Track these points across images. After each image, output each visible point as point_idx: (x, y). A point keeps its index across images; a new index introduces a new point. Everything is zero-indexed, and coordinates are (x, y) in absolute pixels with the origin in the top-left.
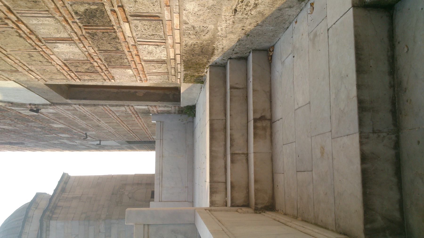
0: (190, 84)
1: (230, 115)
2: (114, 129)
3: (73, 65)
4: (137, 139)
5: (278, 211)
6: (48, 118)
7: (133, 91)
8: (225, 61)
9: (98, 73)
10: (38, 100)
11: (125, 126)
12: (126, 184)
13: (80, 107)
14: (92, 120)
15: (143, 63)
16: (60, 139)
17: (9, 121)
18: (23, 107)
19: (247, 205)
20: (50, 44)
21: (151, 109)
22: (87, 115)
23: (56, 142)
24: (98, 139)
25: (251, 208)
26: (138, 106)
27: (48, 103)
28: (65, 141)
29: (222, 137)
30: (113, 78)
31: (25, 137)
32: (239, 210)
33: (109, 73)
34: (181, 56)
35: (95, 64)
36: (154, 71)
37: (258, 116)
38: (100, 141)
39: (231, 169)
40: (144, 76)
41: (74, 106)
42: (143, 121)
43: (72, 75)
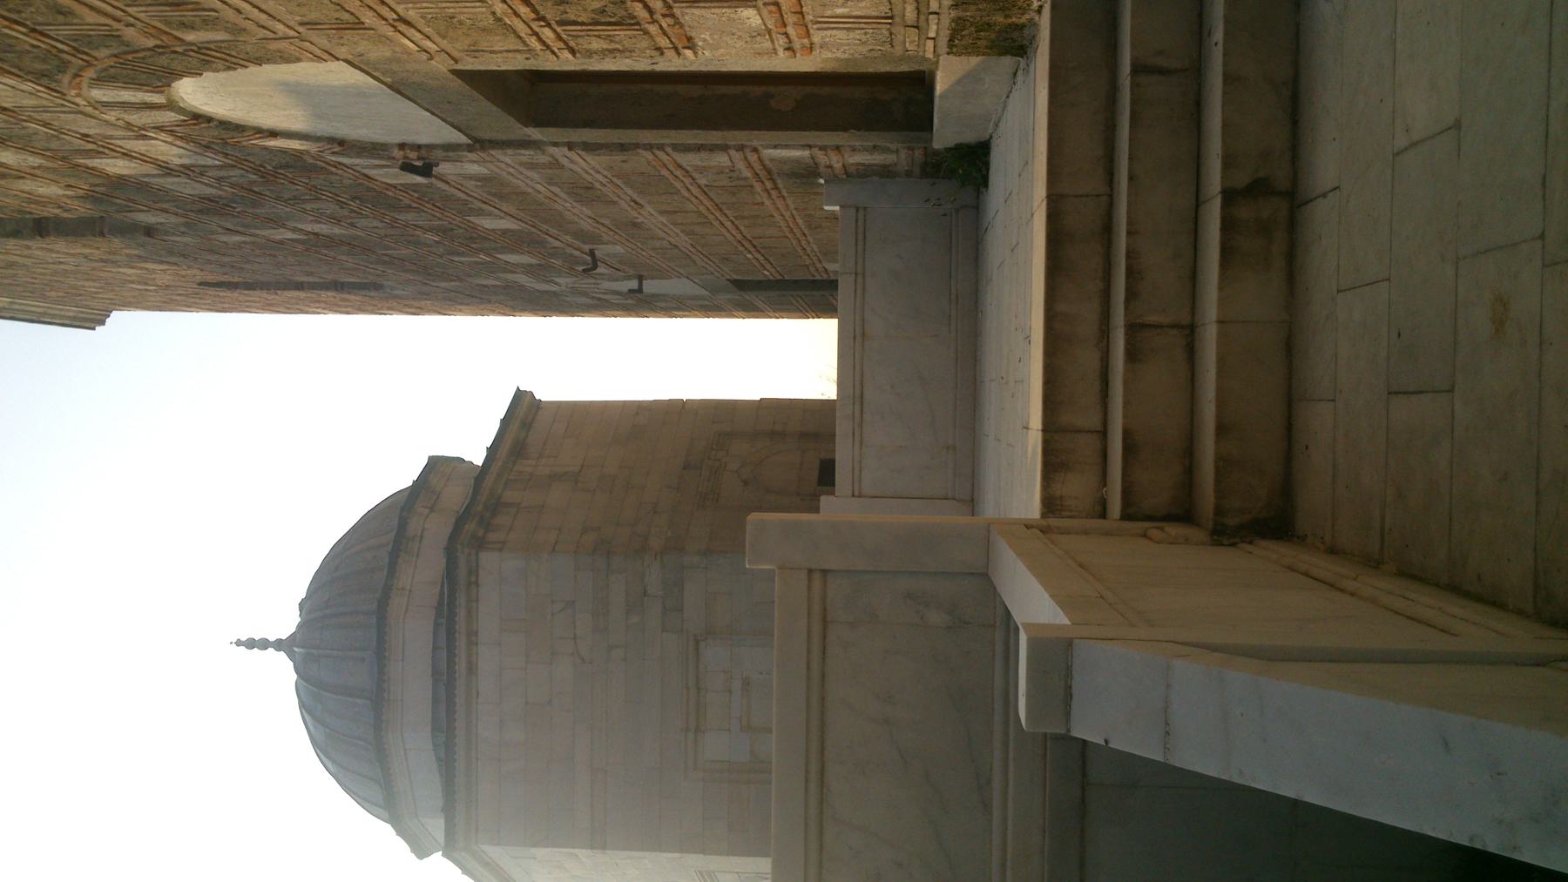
0: (975, 60)
1: (1131, 178)
4: (768, 274)
5: (1303, 538)
6: (463, 196)
7: (757, 91)
9: (638, 24)
10: (428, 129)
11: (728, 224)
13: (572, 155)
14: (615, 203)
16: (505, 271)
17: (331, 208)
18: (382, 158)
19: (1182, 513)
21: (822, 158)
22: (597, 185)
23: (491, 282)
24: (632, 272)
25: (1198, 525)
26: (775, 147)
27: (463, 139)
28: (522, 279)
30: (691, 44)
31: (385, 262)
32: (1154, 533)
33: (678, 23)
36: (839, 11)
37: (1242, 179)
38: (640, 278)
39: (1125, 382)
40: (802, 31)
41: (552, 150)
43: (547, 34)
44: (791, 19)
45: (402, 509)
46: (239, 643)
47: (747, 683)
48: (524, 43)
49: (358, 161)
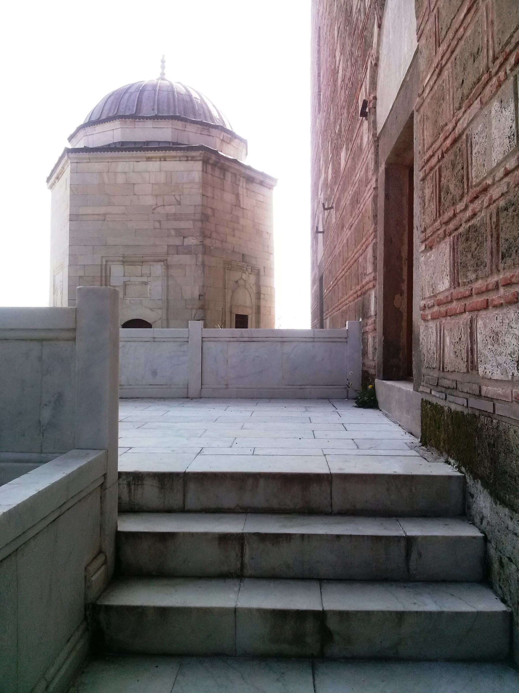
2: (339, 253)
3: (456, 156)
6: (354, 139)
7: (404, 287)
8: (477, 520)
9: (440, 215)
10: (383, 111)
11: (343, 273)
14: (351, 216)
15: (467, 316)
16: (326, 168)
18: (370, 89)
20: (512, 87)
21: (370, 321)
22: (359, 205)
26: (375, 297)
29: (290, 504)
34: (490, 415)
35: (460, 206)
36: (448, 340)
37: (332, 624)
38: (323, 232)
39: (205, 534)
42: (350, 304)
43: (434, 160)
44: (443, 309)
46: (163, 56)
47: (146, 283)
48: (428, 149)
49: (368, 83)
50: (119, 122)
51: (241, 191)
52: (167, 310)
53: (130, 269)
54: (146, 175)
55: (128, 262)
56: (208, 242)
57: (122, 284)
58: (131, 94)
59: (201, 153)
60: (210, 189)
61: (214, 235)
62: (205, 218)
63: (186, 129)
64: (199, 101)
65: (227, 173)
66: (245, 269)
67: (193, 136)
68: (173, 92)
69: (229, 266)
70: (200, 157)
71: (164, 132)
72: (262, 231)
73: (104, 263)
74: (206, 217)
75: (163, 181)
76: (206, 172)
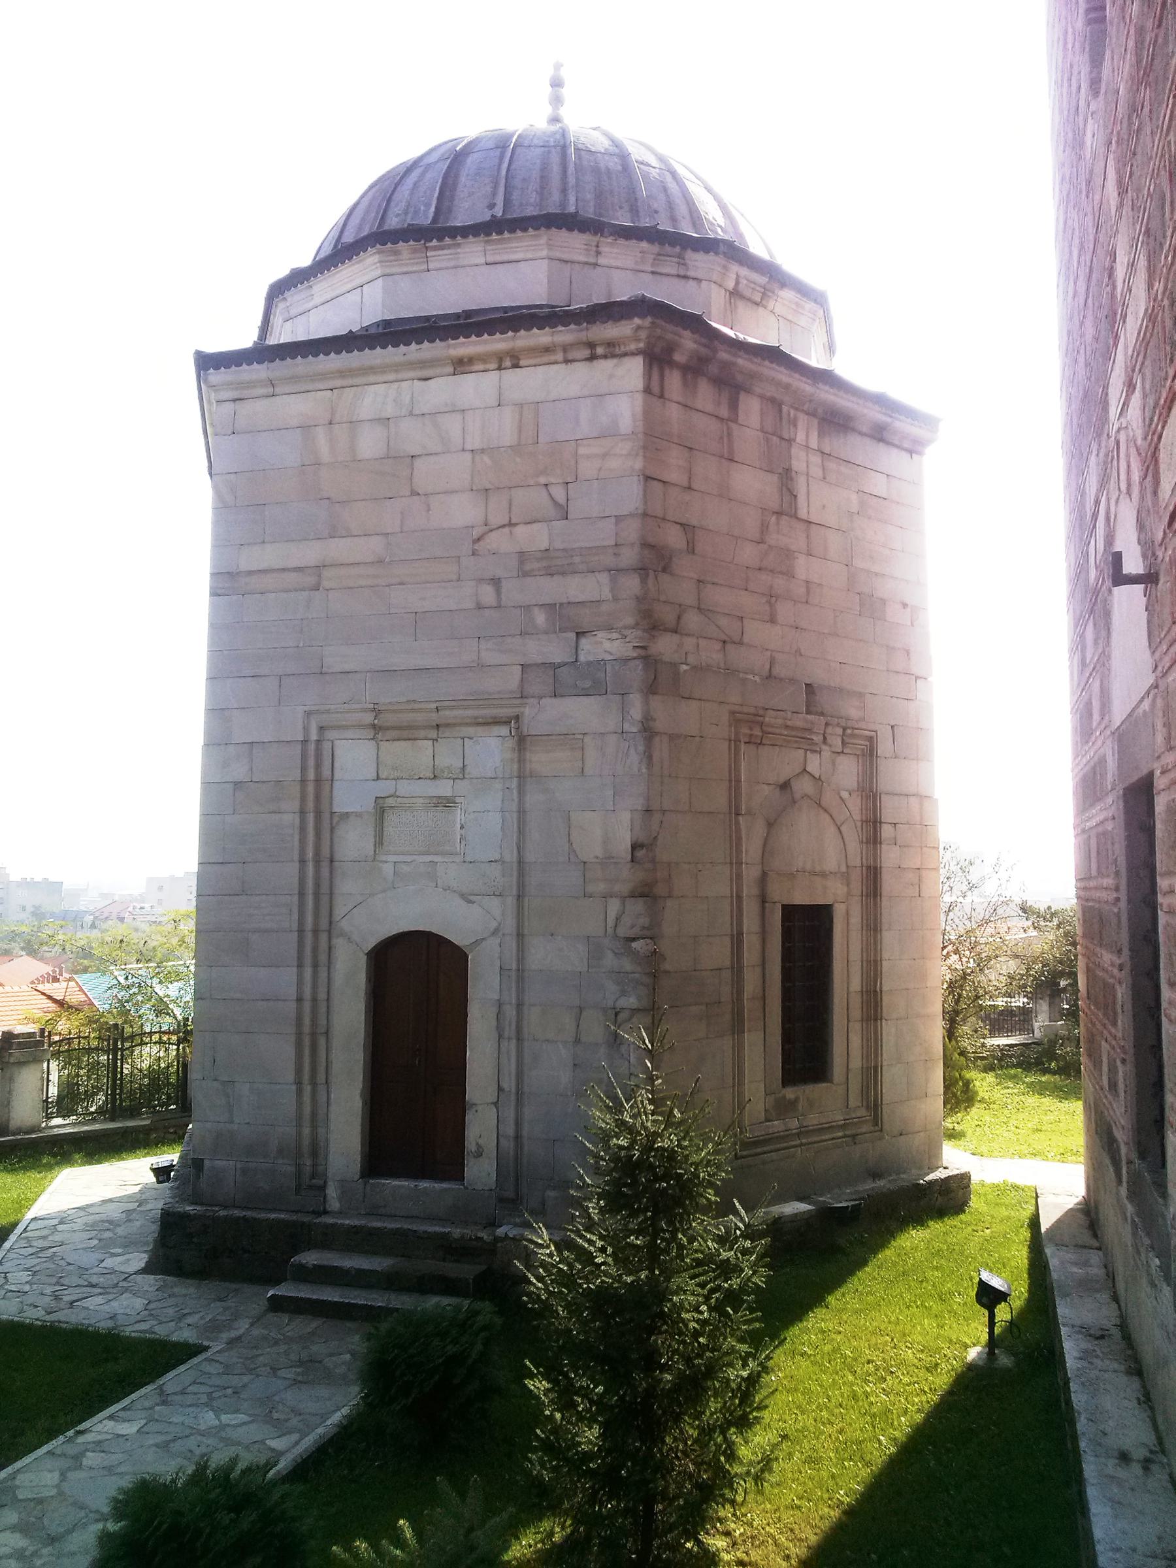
12: (869, 754)
38: (1149, 579)
45: (730, 245)
46: (558, 66)
47: (446, 803)
50: (376, 258)
51: (799, 461)
52: (519, 897)
53: (396, 751)
54: (453, 425)
55: (388, 728)
56: (665, 646)
57: (370, 805)
58: (429, 166)
59: (639, 328)
60: (675, 458)
61: (693, 620)
62: (655, 561)
63: (602, 261)
64: (654, 173)
65: (743, 397)
66: (817, 739)
67: (622, 274)
68: (564, 148)
69: (752, 729)
70: (638, 340)
71: (522, 273)
72: (883, 602)
73: (314, 736)
74: (656, 558)
75: (508, 437)
76: (661, 396)
